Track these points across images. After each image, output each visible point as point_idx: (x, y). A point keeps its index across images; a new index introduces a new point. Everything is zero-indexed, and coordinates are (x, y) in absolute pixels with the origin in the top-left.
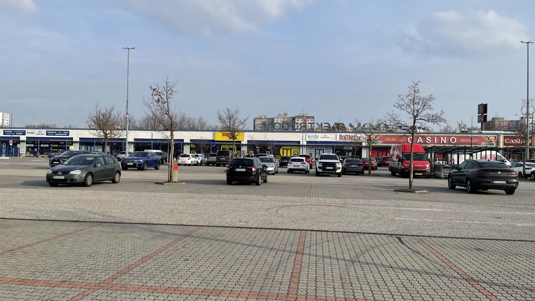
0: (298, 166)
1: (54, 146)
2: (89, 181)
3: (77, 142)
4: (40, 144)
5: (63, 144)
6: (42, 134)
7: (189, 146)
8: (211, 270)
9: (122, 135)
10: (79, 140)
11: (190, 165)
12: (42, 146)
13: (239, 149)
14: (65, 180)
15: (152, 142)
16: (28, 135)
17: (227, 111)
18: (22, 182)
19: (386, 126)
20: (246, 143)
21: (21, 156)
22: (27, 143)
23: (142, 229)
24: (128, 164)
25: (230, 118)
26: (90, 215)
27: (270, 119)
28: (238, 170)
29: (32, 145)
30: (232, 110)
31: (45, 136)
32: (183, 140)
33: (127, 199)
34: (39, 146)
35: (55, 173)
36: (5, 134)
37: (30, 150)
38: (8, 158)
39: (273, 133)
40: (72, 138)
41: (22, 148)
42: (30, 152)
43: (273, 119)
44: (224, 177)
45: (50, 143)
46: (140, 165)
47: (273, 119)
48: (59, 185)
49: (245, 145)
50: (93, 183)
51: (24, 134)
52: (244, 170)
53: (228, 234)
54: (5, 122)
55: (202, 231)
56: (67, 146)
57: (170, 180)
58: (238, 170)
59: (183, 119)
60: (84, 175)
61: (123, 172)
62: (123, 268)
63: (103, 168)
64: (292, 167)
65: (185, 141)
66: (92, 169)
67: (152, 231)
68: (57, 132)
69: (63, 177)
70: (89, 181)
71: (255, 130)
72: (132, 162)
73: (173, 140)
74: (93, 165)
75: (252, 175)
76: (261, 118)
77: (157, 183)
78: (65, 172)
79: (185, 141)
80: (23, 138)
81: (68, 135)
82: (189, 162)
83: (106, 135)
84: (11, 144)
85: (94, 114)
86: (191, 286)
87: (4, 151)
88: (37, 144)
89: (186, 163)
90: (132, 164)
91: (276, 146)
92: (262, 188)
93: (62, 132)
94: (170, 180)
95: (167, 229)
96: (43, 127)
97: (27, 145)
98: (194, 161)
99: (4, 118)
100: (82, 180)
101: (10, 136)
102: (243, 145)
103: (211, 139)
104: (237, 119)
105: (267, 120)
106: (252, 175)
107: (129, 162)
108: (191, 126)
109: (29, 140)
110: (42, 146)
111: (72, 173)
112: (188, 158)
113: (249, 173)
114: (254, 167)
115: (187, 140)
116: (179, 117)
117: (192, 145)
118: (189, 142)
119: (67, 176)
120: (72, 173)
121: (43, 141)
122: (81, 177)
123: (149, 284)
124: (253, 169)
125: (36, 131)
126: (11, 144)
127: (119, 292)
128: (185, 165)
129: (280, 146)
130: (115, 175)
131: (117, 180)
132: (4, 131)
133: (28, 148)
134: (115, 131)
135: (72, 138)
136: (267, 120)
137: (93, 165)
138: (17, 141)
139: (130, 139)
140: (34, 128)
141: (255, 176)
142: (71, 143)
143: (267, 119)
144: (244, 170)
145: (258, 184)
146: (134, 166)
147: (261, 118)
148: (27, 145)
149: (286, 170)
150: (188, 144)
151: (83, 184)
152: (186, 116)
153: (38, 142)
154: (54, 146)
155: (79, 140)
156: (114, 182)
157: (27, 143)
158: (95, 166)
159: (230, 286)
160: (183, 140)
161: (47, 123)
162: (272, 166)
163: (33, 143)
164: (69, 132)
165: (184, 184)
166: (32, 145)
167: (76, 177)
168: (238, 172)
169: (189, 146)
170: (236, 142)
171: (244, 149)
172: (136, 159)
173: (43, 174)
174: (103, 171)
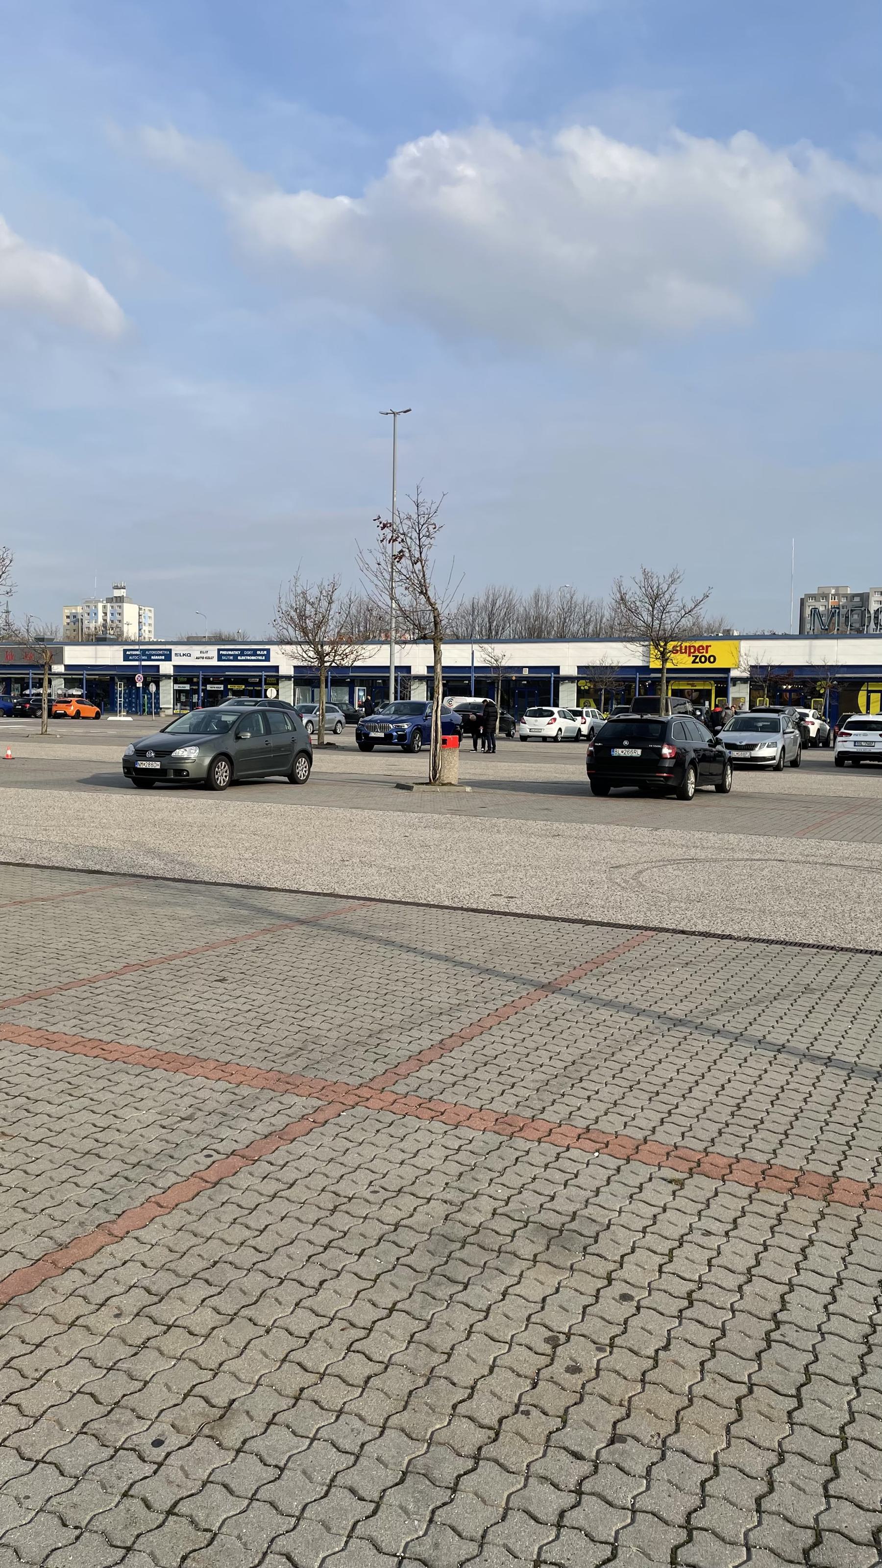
0: (870, 743)
1: (236, 687)
2: (222, 775)
3: (288, 678)
4: (204, 684)
5: (254, 683)
6: (206, 657)
7: (573, 687)
8: (692, 1079)
9: (722, 655)
10: (172, 673)
11: (555, 739)
12: (209, 687)
13: (723, 692)
14: (162, 772)
15: (473, 675)
16: (177, 661)
17: (642, 577)
18: (87, 775)
19: (439, 615)
20: (746, 675)
21: (162, 714)
22: (176, 682)
23: (226, 899)
24: (372, 734)
25: (655, 598)
26: (142, 860)
27: (854, 596)
28: (619, 752)
29: (187, 687)
30: (661, 573)
31: (215, 662)
32: (557, 669)
33: (335, 832)
34: (201, 687)
35: (141, 753)
36: (126, 658)
37: (183, 699)
38: (130, 719)
39: (834, 642)
40: (276, 668)
41: (167, 692)
42: (184, 704)
43: (864, 598)
44: (579, 773)
45: (227, 681)
46: (401, 738)
47: (864, 598)
48: (157, 784)
49: (743, 680)
50: (234, 783)
51: (168, 658)
52: (638, 753)
53: (358, 916)
54: (146, 628)
55: (260, 899)
56: (264, 687)
57: (434, 779)
58: (619, 752)
59: (568, 610)
60: (207, 761)
61: (317, 756)
62: (426, 1044)
63: (259, 743)
64: (849, 747)
65: (563, 672)
66: (231, 746)
67: (237, 903)
68: (242, 650)
69: (157, 765)
70: (222, 775)
71: (802, 635)
72: (382, 729)
73: (439, 670)
74: (232, 733)
75: (662, 769)
76: (825, 596)
77: (400, 786)
78: (163, 752)
79: (414, 672)
80: (166, 668)
81: (268, 659)
82: (552, 731)
83: (321, 656)
84: (139, 685)
85: (290, 600)
86: (629, 1131)
87: (120, 700)
88: (197, 684)
89: (544, 733)
90: (382, 735)
91: (841, 681)
92: (701, 808)
93: (254, 652)
94: (434, 779)
95: (279, 903)
96: (217, 640)
97: (177, 687)
98: (567, 729)
99: (143, 620)
100: (204, 774)
101: (137, 663)
102: (735, 681)
103: (640, 664)
104: (671, 600)
105: (843, 601)
106: (662, 769)
107: (374, 729)
108: (591, 627)
109: (183, 674)
110: (209, 687)
111: (179, 753)
112: (548, 719)
113: (653, 759)
114: (670, 745)
115: (568, 669)
116: (556, 602)
117: (582, 682)
118: (574, 673)
119: (166, 760)
120: (179, 753)
121: (209, 674)
122: (200, 765)
123: (499, 1106)
124: (666, 751)
125: (196, 650)
126: (139, 685)
127: (412, 1122)
128: (545, 739)
129: (857, 684)
130: (296, 761)
131: (301, 773)
132: (125, 651)
133: (178, 693)
134: (343, 647)
135: (276, 668)
136: (843, 601)
137: (232, 733)
138: (154, 676)
139: (568, 669)
140: (191, 641)
141: (670, 770)
142: (273, 680)
143: (845, 596)
144: (638, 753)
145: (683, 796)
146: (388, 739)
147: (825, 596)
148: (177, 687)
149: (829, 756)
150: (571, 679)
151: (205, 783)
152: (578, 598)
153: (198, 677)
154: (236, 687)
155: (172, 673)
156: (293, 780)
157: (176, 682)
158: (238, 738)
159: (700, 1134)
160: (557, 669)
161: (228, 629)
162: (774, 745)
163: (189, 681)
164: (268, 650)
165: (468, 789)
166: (187, 687)
167: (188, 766)
168: (620, 758)
169: (573, 687)
170: (670, 671)
171: (740, 693)
172: (392, 722)
173: (114, 756)
174: (263, 751)
